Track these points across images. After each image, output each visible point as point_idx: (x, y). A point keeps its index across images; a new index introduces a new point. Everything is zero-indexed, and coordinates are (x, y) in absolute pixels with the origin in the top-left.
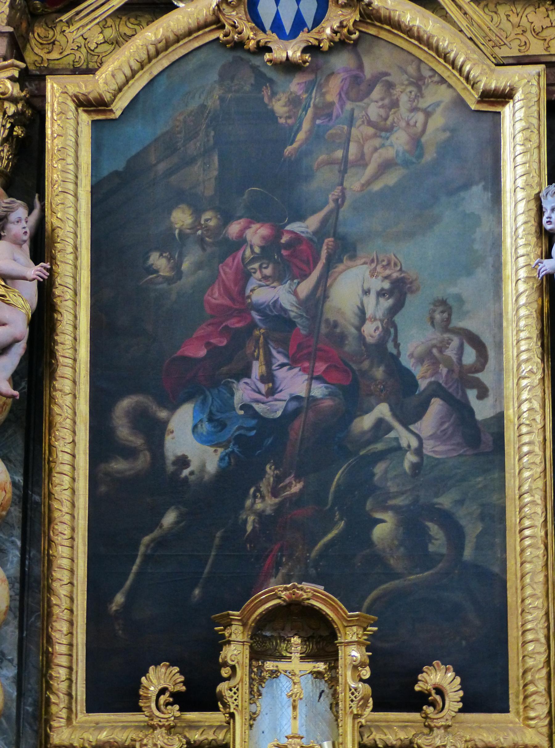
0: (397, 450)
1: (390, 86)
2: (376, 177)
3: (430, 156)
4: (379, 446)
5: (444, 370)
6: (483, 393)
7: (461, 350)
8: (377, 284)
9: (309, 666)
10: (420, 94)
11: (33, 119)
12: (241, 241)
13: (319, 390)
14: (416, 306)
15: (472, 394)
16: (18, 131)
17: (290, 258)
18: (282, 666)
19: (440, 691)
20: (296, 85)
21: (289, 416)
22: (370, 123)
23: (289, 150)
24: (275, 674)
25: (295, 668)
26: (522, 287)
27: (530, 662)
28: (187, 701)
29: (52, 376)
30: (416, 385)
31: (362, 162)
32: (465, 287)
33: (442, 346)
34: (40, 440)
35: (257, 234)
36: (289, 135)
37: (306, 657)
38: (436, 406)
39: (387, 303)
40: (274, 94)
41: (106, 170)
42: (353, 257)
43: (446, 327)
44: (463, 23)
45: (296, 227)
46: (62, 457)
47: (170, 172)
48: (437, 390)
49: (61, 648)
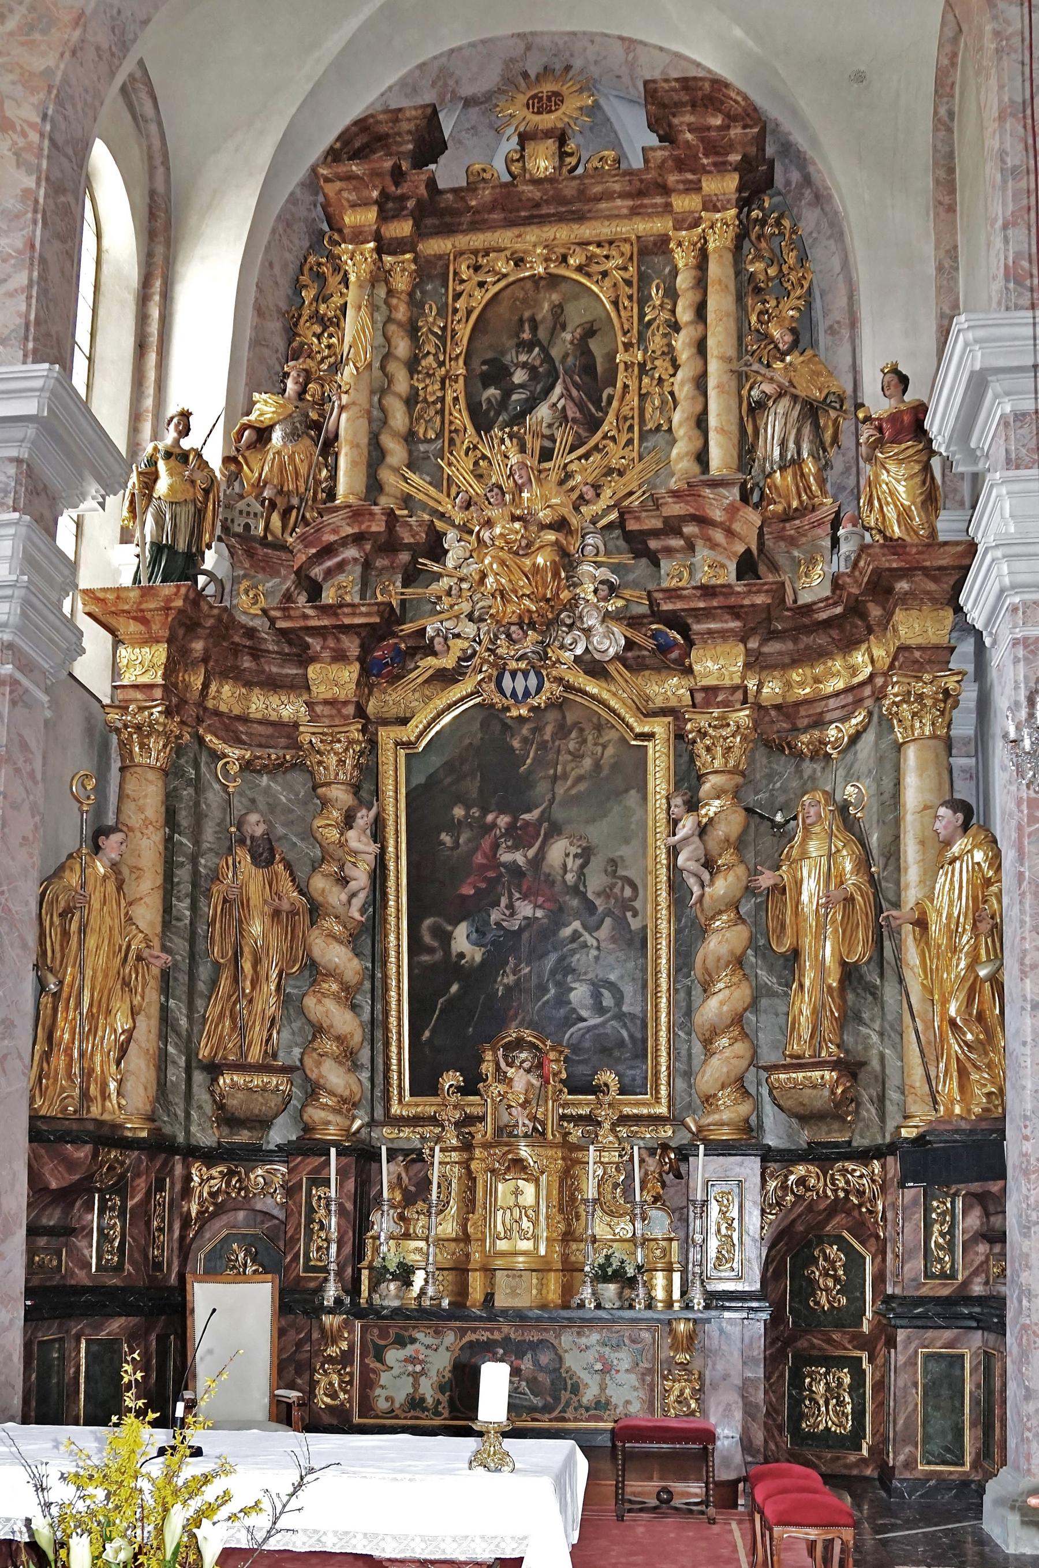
2: (573, 786)
3: (606, 771)
6: (635, 915)
7: (623, 889)
8: (573, 850)
10: (600, 735)
11: (373, 743)
12: (494, 825)
13: (539, 914)
14: (597, 864)
15: (629, 914)
17: (519, 836)
19: (606, 1085)
21: (521, 930)
22: (570, 753)
31: (565, 776)
32: (625, 851)
33: (612, 887)
35: (503, 821)
38: (608, 921)
39: (579, 862)
41: (414, 783)
42: (560, 834)
45: (526, 816)
47: (451, 784)
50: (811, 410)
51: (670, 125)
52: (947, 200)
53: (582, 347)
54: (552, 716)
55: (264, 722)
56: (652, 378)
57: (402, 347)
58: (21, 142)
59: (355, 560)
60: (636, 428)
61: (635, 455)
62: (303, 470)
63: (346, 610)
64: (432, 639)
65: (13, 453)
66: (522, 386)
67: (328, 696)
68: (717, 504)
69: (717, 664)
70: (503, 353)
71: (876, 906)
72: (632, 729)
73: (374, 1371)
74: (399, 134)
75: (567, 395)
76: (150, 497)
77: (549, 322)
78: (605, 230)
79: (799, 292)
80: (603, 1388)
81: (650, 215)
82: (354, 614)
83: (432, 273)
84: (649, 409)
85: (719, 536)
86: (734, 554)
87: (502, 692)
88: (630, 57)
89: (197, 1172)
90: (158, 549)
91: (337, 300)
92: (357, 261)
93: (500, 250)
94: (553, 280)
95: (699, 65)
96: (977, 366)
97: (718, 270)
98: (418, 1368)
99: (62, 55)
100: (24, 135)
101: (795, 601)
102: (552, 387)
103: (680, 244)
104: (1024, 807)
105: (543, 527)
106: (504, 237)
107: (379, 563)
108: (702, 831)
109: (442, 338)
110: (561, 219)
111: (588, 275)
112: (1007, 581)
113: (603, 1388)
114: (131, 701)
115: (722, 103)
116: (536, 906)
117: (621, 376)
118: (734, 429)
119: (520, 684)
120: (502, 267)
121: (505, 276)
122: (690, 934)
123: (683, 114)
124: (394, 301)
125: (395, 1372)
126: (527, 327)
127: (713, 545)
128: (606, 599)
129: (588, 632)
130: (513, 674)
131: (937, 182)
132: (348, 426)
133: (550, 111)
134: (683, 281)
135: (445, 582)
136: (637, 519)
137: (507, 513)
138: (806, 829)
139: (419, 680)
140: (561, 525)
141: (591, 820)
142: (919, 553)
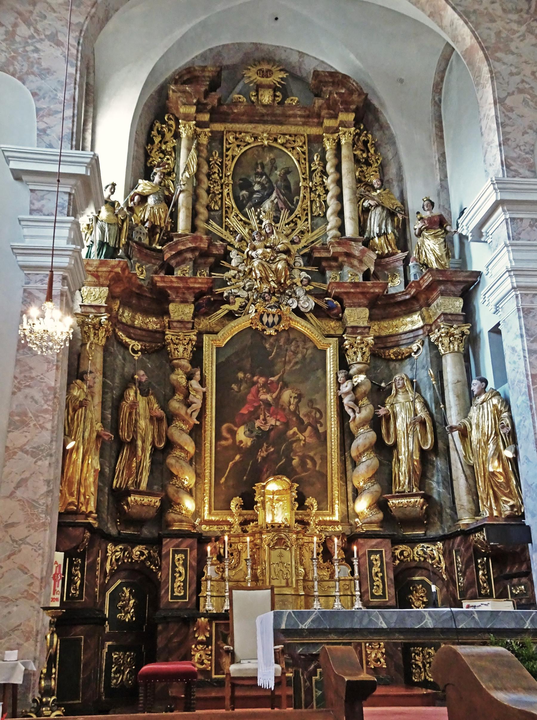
0: (299, 440)
2: (293, 366)
3: (308, 360)
6: (321, 426)
7: (316, 413)
8: (294, 395)
10: (305, 344)
12: (257, 382)
13: (278, 423)
14: (304, 401)
15: (318, 425)
16: (195, 349)
17: (268, 388)
21: (270, 430)
31: (290, 361)
32: (317, 397)
33: (311, 412)
35: (262, 380)
38: (309, 428)
39: (296, 400)
41: (220, 361)
42: (287, 387)
45: (272, 379)
48: (309, 424)
51: (321, 90)
53: (284, 178)
54: (284, 335)
55: (141, 329)
56: (316, 194)
59: (191, 258)
60: (309, 215)
62: (163, 216)
65: (68, 190)
66: (258, 191)
67: (179, 318)
70: (249, 176)
74: (204, 77)
77: (269, 166)
78: (293, 129)
79: (376, 165)
81: (311, 126)
82: (195, 282)
83: (217, 138)
85: (356, 262)
86: (362, 271)
87: (262, 321)
88: (301, 60)
90: (102, 244)
91: (170, 145)
93: (247, 133)
94: (271, 148)
95: (332, 67)
96: (499, 199)
97: (345, 152)
99: (87, 18)
102: (271, 193)
103: (328, 140)
104: (530, 377)
106: (249, 127)
107: (199, 261)
108: (354, 389)
109: (221, 167)
110: (273, 123)
111: (286, 148)
112: (515, 285)
116: (277, 420)
117: (302, 192)
119: (271, 320)
120: (248, 139)
121: (249, 144)
122: (347, 436)
123: (328, 87)
124: (202, 148)
126: (259, 166)
127: (352, 266)
128: (306, 286)
129: (298, 299)
130: (268, 315)
131: (436, 127)
133: (267, 77)
134: (329, 156)
135: (232, 273)
136: (319, 252)
137: (263, 245)
138: (397, 391)
139: (222, 315)
140: (287, 252)
141: (302, 382)
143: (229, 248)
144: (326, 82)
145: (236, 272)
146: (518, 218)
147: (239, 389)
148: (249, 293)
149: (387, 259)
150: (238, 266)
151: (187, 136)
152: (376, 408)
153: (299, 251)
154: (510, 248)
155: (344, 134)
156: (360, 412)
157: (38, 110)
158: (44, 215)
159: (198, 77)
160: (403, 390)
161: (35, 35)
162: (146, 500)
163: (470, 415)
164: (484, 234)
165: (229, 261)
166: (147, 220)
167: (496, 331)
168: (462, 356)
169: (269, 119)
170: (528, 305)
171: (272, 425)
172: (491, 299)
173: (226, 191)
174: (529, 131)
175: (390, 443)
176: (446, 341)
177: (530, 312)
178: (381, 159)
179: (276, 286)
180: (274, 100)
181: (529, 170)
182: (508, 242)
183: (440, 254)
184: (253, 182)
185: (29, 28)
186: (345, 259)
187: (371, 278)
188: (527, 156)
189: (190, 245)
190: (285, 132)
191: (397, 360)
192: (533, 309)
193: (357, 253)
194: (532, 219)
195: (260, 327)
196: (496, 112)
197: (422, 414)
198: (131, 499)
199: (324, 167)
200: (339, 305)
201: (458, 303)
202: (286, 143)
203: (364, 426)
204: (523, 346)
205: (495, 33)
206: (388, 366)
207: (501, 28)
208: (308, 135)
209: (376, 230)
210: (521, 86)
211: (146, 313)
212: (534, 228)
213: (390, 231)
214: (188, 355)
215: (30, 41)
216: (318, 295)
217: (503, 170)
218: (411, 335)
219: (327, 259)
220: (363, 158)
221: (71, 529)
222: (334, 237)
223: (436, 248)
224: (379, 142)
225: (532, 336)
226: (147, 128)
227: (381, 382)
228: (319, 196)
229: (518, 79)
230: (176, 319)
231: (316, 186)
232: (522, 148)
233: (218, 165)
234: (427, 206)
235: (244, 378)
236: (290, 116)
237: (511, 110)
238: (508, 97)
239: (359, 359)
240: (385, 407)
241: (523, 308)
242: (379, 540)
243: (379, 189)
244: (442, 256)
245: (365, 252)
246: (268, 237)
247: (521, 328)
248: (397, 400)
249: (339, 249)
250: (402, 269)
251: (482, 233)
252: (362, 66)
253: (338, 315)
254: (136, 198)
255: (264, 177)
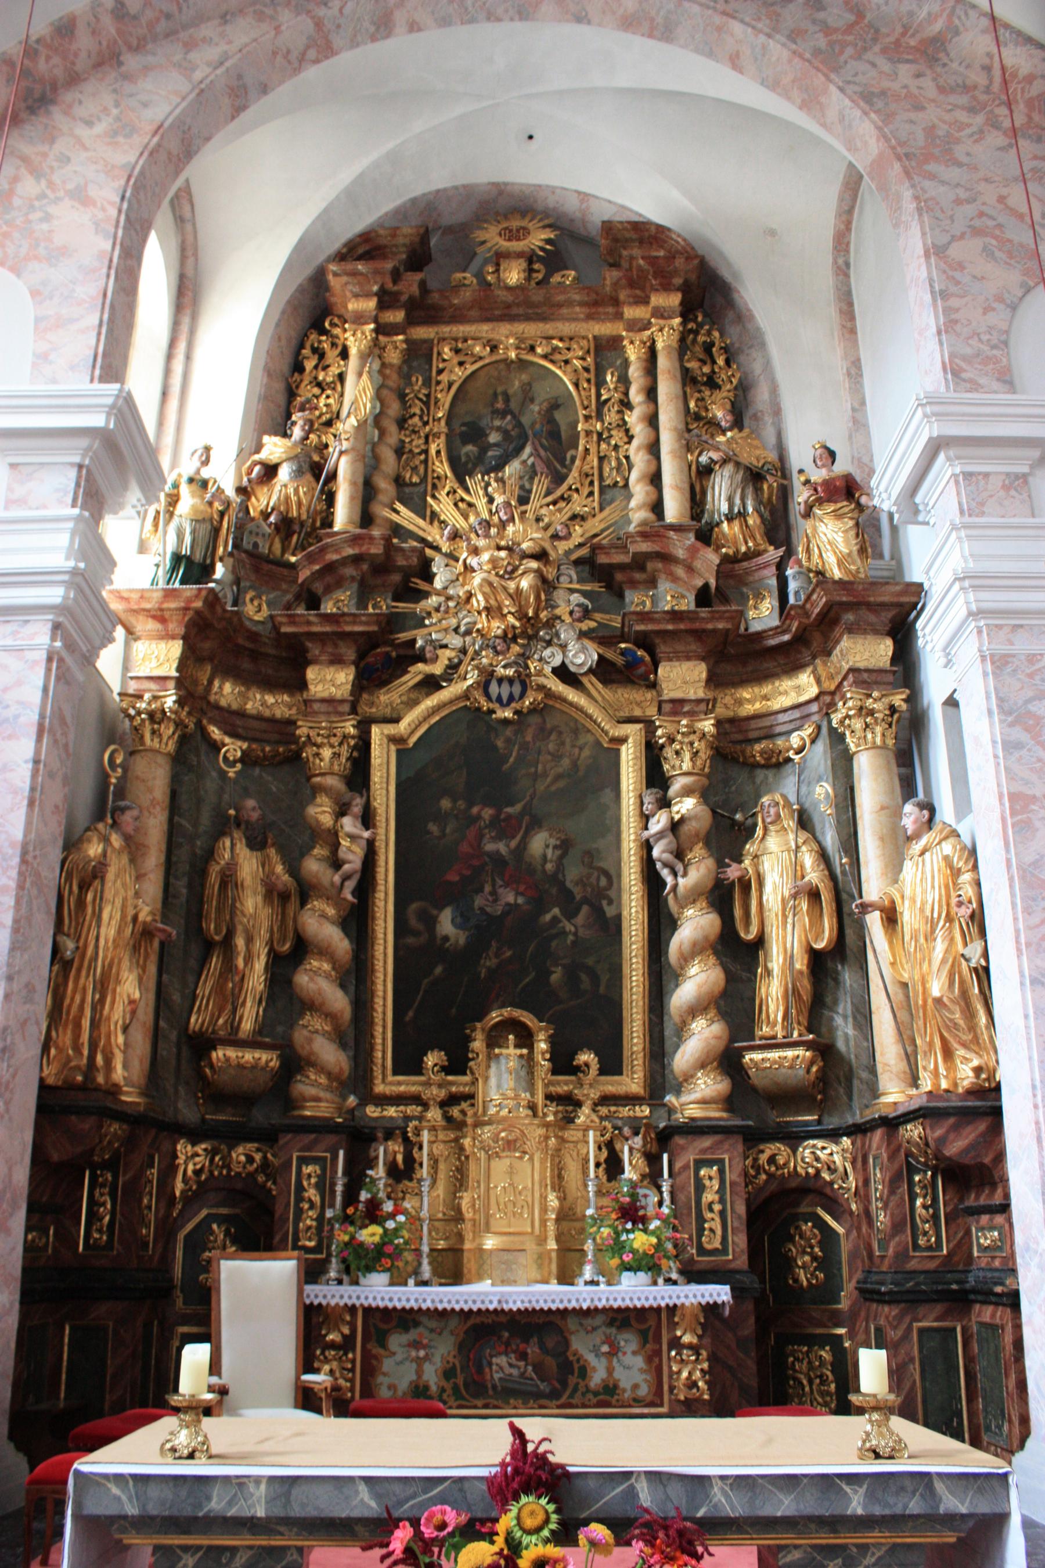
0: (564, 933)
1: (560, 733)
3: (581, 773)
4: (554, 931)
5: (589, 890)
8: (553, 842)
9: (518, 1052)
10: (577, 738)
11: (364, 745)
12: (479, 817)
13: (520, 900)
15: (604, 903)
16: (355, 754)
17: (503, 828)
18: (504, 1051)
20: (509, 732)
21: (505, 914)
22: (549, 753)
23: (506, 767)
24: (498, 1056)
25: (511, 1053)
26: (632, 845)
27: (635, 1049)
28: (447, 1070)
29: (374, 891)
30: (574, 898)
31: (545, 775)
34: (366, 925)
35: (488, 813)
36: (505, 759)
37: (517, 1046)
38: (585, 909)
39: (558, 852)
40: (497, 736)
42: (540, 827)
43: (590, 866)
44: (599, 699)
46: (379, 914)
48: (585, 900)
49: (379, 1041)
50: (754, 477)
52: (849, 325)
56: (609, 444)
57: (394, 408)
58: (100, 215)
59: (353, 578)
60: (596, 484)
61: (596, 504)
63: (347, 619)
64: (423, 648)
66: (495, 445)
68: (681, 545)
69: (683, 677)
70: (480, 418)
71: (838, 895)
72: (606, 733)
73: (376, 1357)
75: (535, 453)
76: (172, 514)
78: (566, 328)
79: (728, 387)
80: (610, 1370)
82: (354, 623)
83: (419, 355)
84: (606, 470)
85: (680, 571)
86: (694, 587)
89: (183, 1148)
91: (334, 370)
92: (356, 340)
96: (935, 435)
97: (664, 363)
98: (422, 1353)
100: (104, 209)
101: (746, 629)
103: (632, 342)
105: (525, 556)
106: (484, 329)
108: (675, 826)
109: (427, 404)
110: (528, 318)
111: (552, 362)
113: (610, 1370)
114: (145, 691)
115: (665, 242)
117: (582, 442)
118: (687, 487)
121: (481, 358)
124: (388, 372)
125: (399, 1357)
126: (500, 398)
127: (675, 579)
128: (580, 620)
129: (563, 647)
132: (345, 469)
133: (519, 240)
134: (635, 372)
135: (433, 600)
136: (607, 554)
137: (493, 544)
138: (766, 829)
139: (411, 683)
140: (541, 556)
142: (864, 590)
143: (429, 552)
144: (627, 240)
145: (442, 599)
146: (979, 474)
147: (443, 831)
148: (468, 639)
149: (745, 564)
150: (446, 588)
151: (359, 351)
152: (721, 864)
153: (568, 553)
154: (963, 533)
155: (661, 330)
156: (685, 875)
157: (38, 320)
158: (30, 508)
159: (385, 247)
160: (778, 827)
161: (48, 192)
162: (249, 1056)
163: (901, 877)
164: (921, 507)
165: (429, 578)
166: (273, 509)
167: (952, 702)
168: (891, 755)
169: (521, 311)
170: (1003, 648)
171: (508, 904)
172: (936, 637)
173: (433, 448)
174: (995, 305)
175: (751, 937)
176: (858, 724)
177: (1007, 663)
178: (738, 375)
179: (517, 624)
180: (528, 279)
181: (998, 380)
182: (957, 521)
183: (846, 551)
184: (503, 430)
185: (38, 182)
186: (660, 565)
187: (715, 600)
188: (995, 352)
189: (350, 551)
190: (551, 333)
191: (767, 766)
192: (1014, 656)
193: (680, 553)
194: (1008, 474)
195: (485, 705)
196: (929, 273)
197: (814, 875)
198: (219, 1054)
199: (626, 394)
200: (647, 658)
201: (882, 646)
202: (554, 354)
203: (694, 902)
204: (992, 734)
205: (924, 129)
206: (752, 778)
207: (936, 121)
208: (595, 337)
209: (724, 508)
210: (977, 223)
211: (270, 685)
212: (1013, 493)
213: (750, 509)
214: (343, 764)
215: (37, 204)
216: (603, 638)
217: (946, 379)
218: (796, 714)
219: (622, 567)
220: (704, 374)
221: (73, 1118)
222: (644, 523)
223: (839, 538)
224: (737, 345)
225: (1010, 713)
226: (294, 343)
227: (736, 812)
228: (616, 447)
229: (970, 210)
230: (320, 695)
231: (609, 430)
232: (985, 338)
233: (420, 400)
234: (821, 458)
235: (452, 809)
236: (560, 305)
237: (961, 266)
238: (955, 245)
239: (687, 766)
240: (740, 862)
241: (992, 656)
242: (313, 1136)
243: (730, 429)
244: (849, 555)
245: (697, 550)
246: (504, 529)
247: (988, 698)
248: (765, 849)
249: (644, 547)
250: (773, 582)
251: (916, 505)
252: (692, 208)
253: (647, 679)
254: (257, 469)
255: (509, 417)
